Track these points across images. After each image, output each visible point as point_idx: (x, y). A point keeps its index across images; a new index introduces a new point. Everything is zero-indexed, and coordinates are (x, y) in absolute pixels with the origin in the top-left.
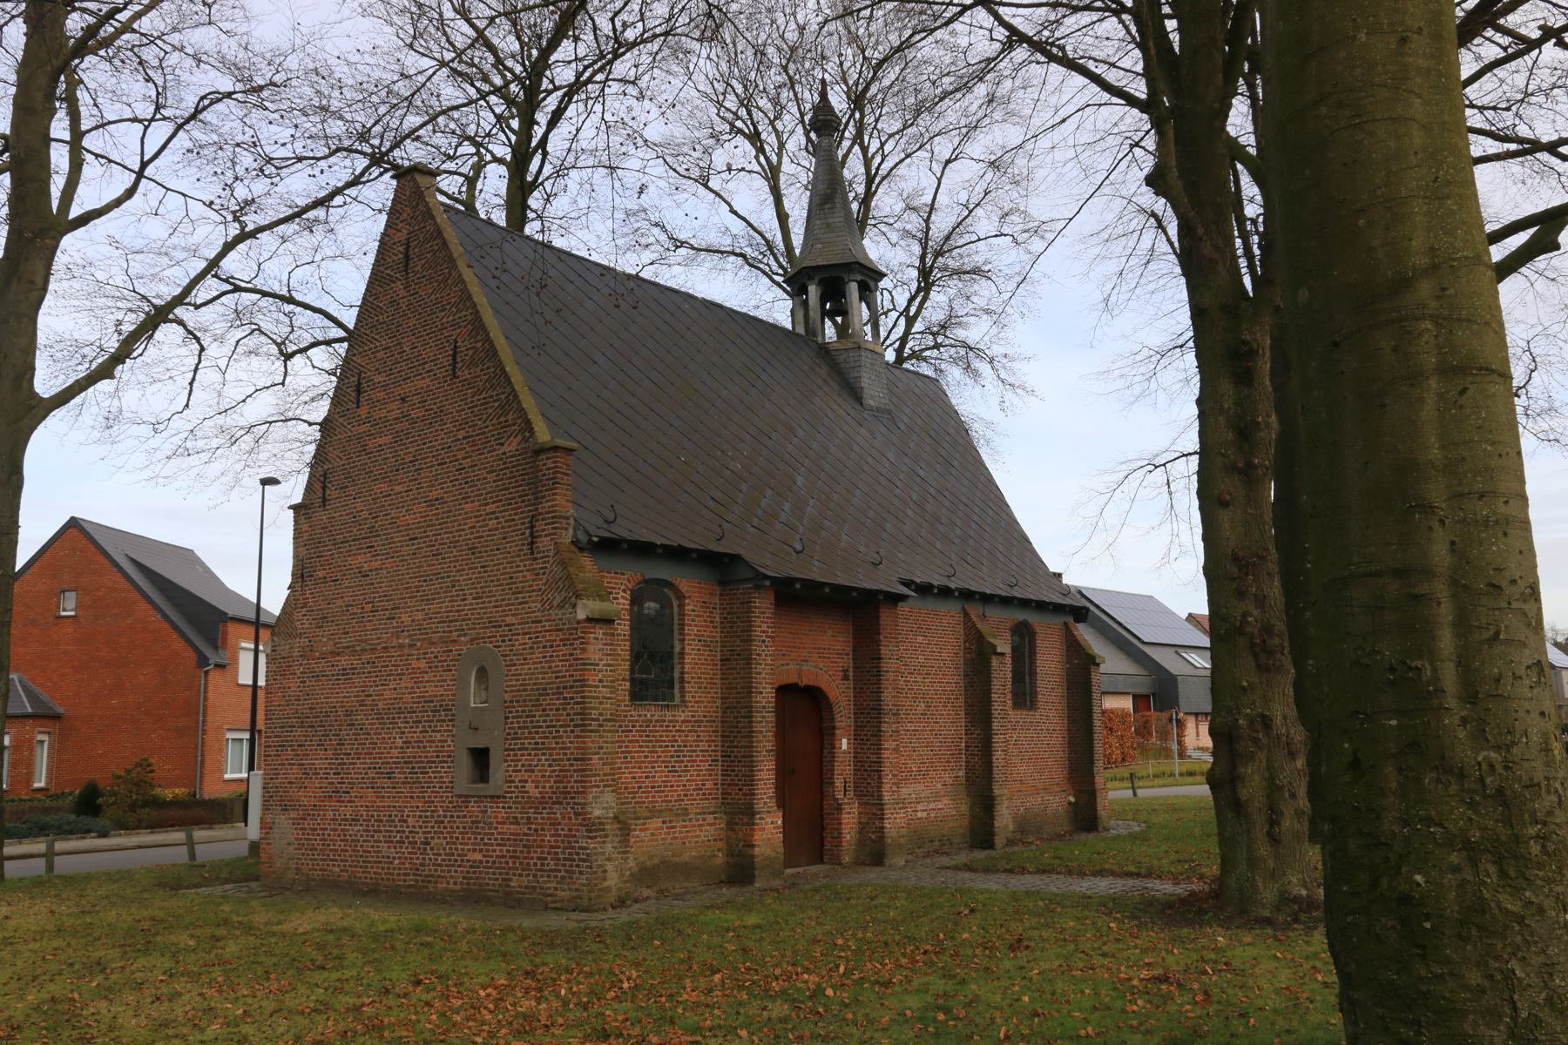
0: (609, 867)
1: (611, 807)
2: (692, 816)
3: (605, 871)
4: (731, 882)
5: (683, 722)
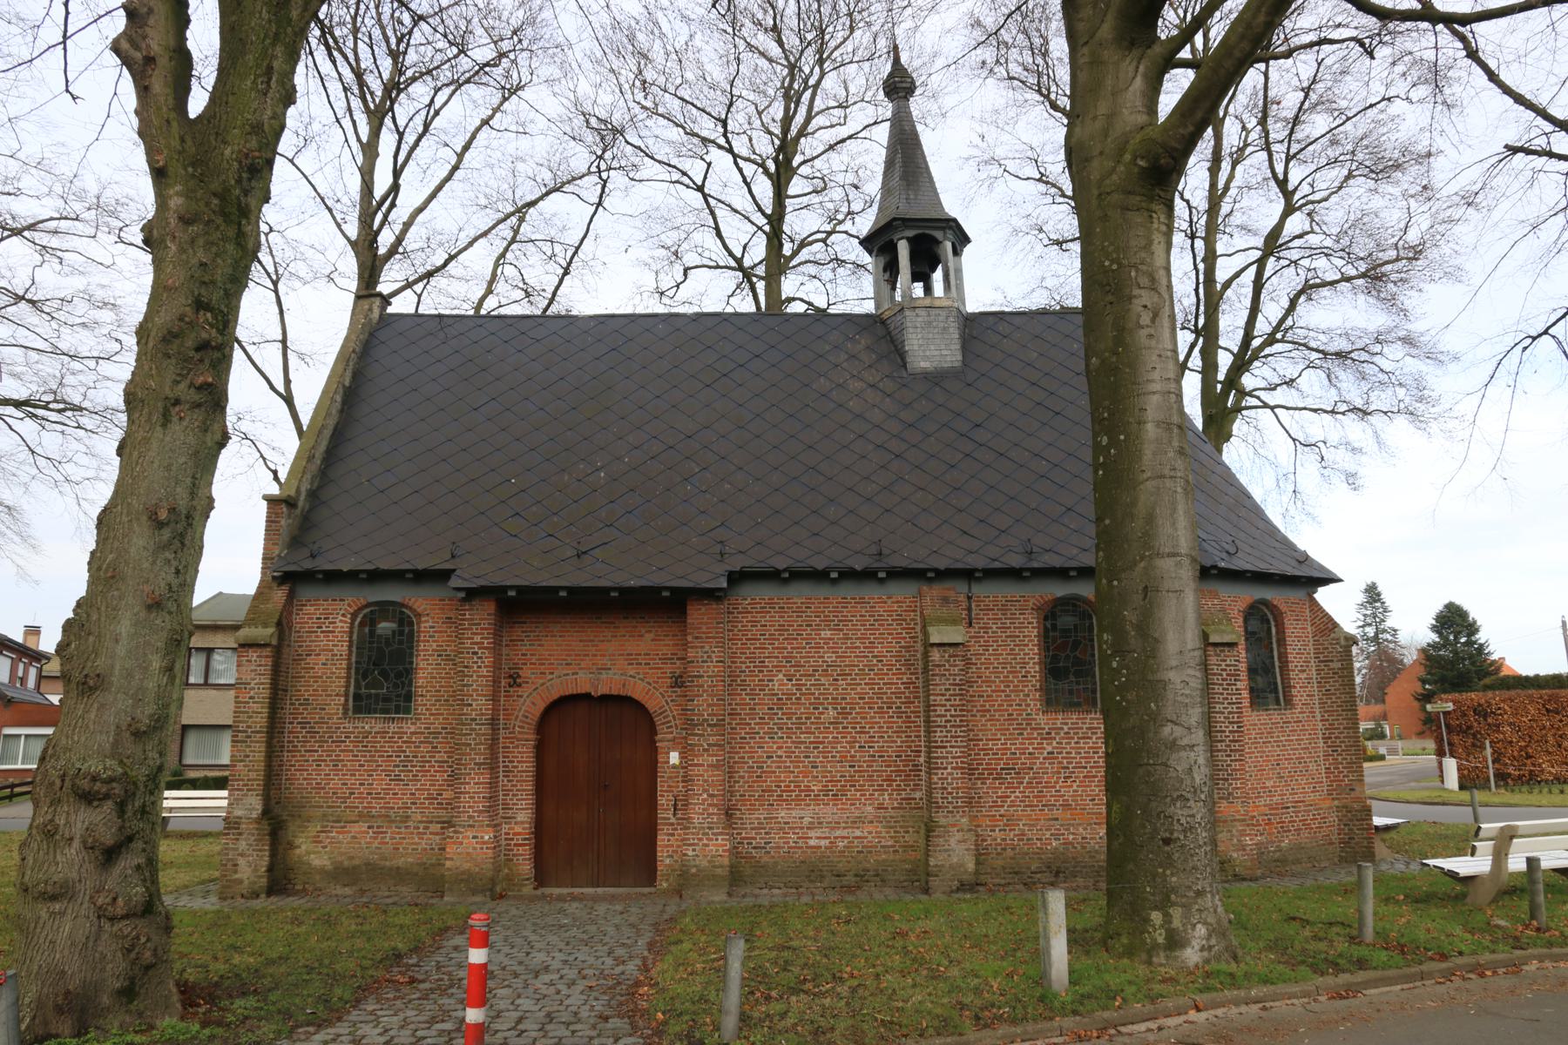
0: (241, 861)
1: (254, 809)
2: (410, 824)
3: (236, 865)
4: (271, 891)
5: (412, 733)
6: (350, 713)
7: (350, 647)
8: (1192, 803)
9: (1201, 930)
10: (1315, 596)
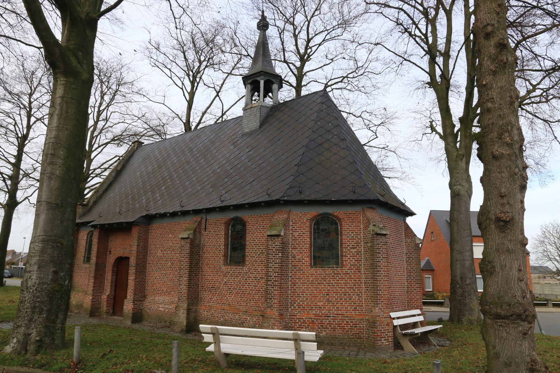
6: (85, 262)
7: (86, 244)
8: (25, 292)
9: (15, 340)
10: (471, 210)
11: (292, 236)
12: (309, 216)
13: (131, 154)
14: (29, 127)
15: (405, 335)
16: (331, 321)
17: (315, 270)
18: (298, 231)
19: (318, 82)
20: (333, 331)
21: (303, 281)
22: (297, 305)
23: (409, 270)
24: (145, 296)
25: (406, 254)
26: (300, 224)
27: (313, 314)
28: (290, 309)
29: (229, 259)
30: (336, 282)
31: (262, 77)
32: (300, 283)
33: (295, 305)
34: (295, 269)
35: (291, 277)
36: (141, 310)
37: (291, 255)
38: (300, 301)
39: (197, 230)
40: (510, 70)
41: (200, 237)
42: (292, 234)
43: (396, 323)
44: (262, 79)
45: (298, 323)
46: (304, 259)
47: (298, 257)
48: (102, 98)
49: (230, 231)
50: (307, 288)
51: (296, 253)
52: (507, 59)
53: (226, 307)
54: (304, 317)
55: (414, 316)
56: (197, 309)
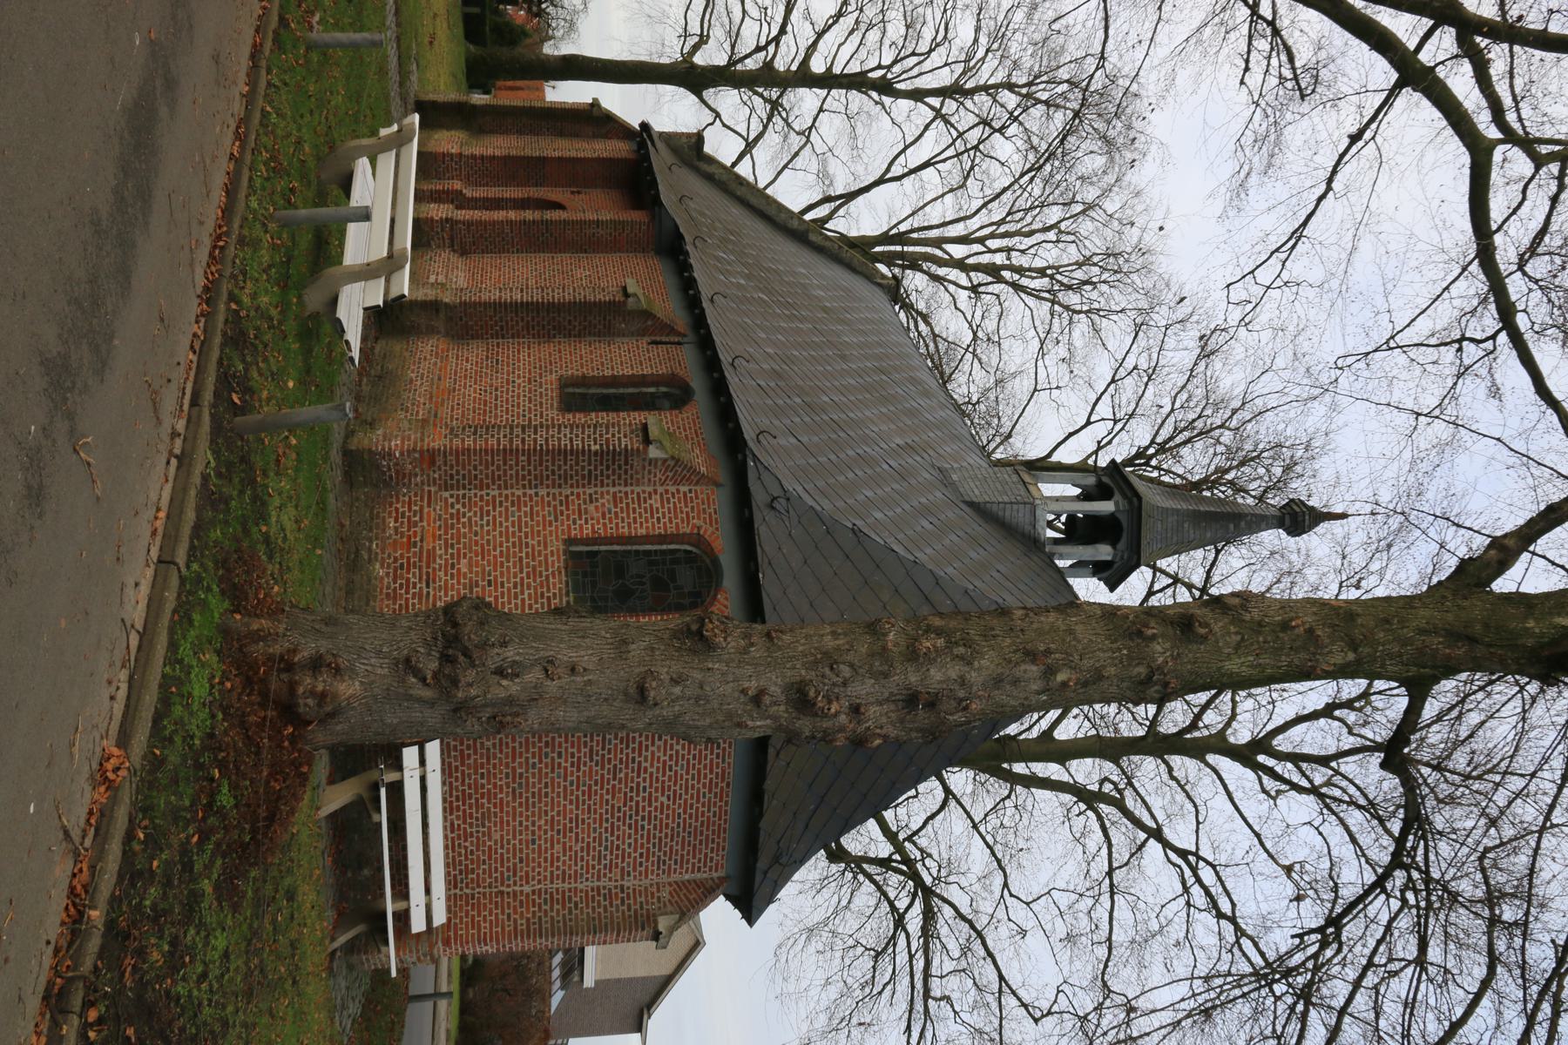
11: (650, 493)
12: (708, 531)
13: (858, 269)
14: (918, 95)
15: (375, 788)
16: (414, 587)
17: (558, 550)
18: (663, 507)
19: (1197, 832)
20: (388, 595)
21: (526, 522)
22: (458, 510)
23: (570, 897)
24: (464, 253)
25: (622, 886)
26: (685, 510)
27: (434, 548)
28: (446, 494)
29: (577, 390)
30: (527, 602)
31: (1123, 504)
32: (520, 517)
33: (457, 507)
34: (557, 503)
35: (537, 494)
36: (429, 245)
37: (596, 493)
38: (470, 518)
39: (649, 323)
40: (1125, 652)
41: (633, 335)
42: (655, 492)
43: (410, 755)
44: (1116, 504)
45: (410, 510)
46: (586, 523)
47: (591, 508)
48: (1042, 272)
49: (652, 390)
50: (507, 532)
51: (603, 505)
52: (1154, 637)
53: (447, 383)
54: (425, 524)
55: (428, 891)
56: (438, 332)
